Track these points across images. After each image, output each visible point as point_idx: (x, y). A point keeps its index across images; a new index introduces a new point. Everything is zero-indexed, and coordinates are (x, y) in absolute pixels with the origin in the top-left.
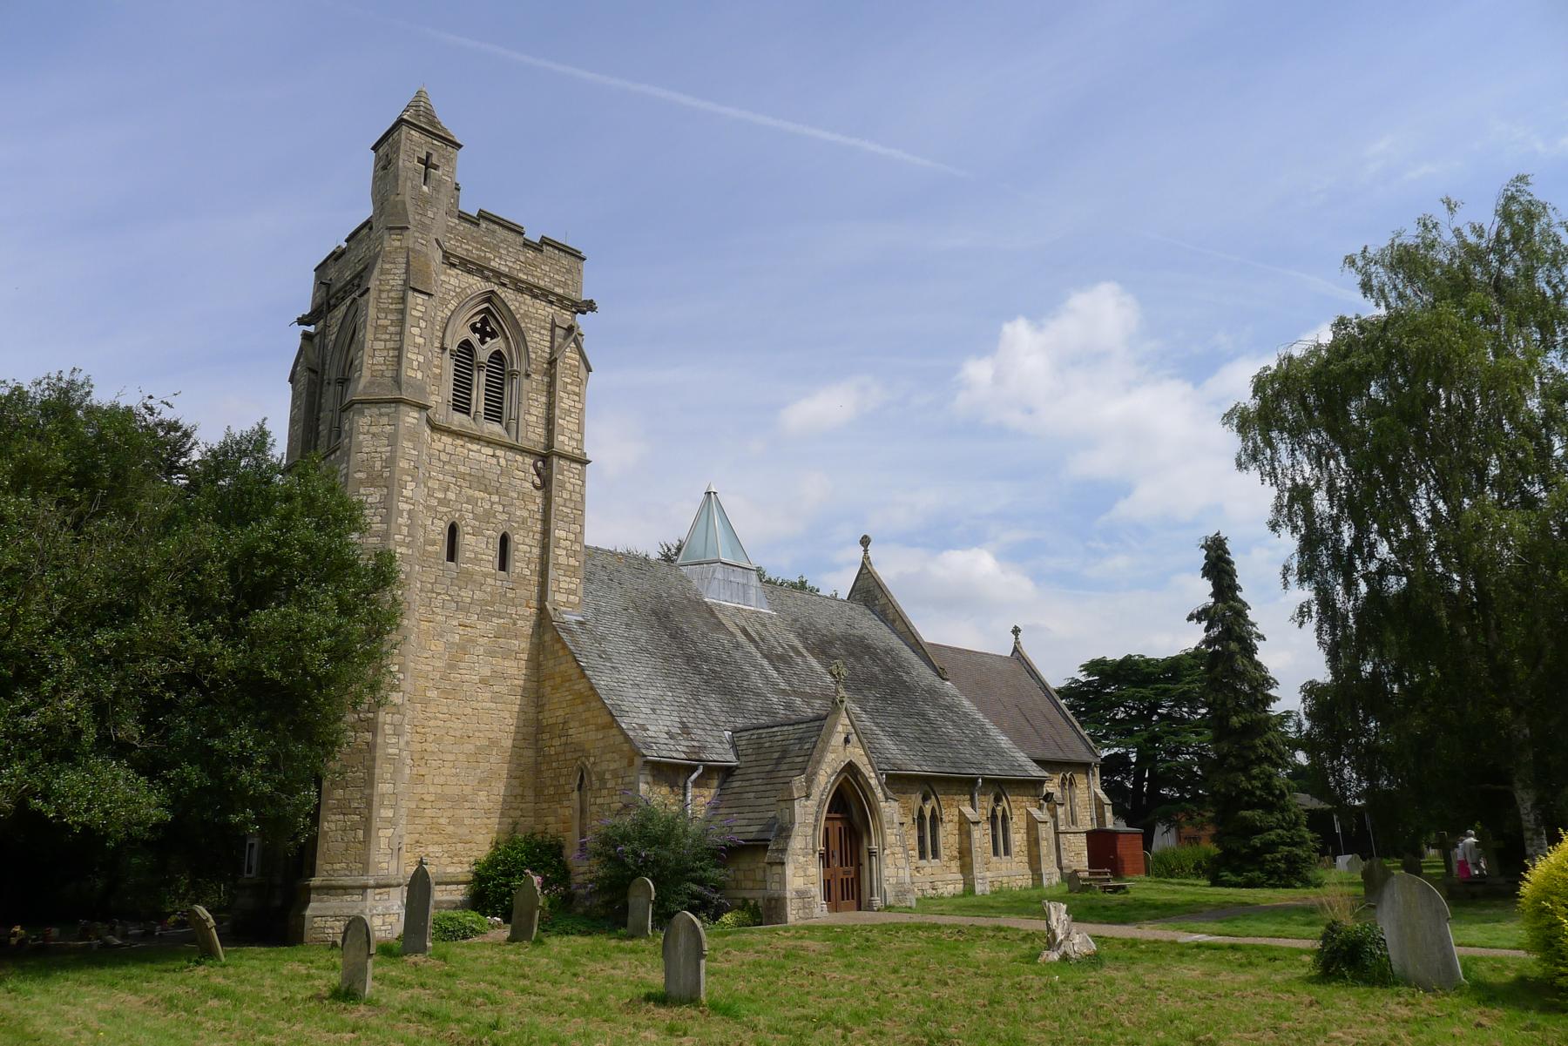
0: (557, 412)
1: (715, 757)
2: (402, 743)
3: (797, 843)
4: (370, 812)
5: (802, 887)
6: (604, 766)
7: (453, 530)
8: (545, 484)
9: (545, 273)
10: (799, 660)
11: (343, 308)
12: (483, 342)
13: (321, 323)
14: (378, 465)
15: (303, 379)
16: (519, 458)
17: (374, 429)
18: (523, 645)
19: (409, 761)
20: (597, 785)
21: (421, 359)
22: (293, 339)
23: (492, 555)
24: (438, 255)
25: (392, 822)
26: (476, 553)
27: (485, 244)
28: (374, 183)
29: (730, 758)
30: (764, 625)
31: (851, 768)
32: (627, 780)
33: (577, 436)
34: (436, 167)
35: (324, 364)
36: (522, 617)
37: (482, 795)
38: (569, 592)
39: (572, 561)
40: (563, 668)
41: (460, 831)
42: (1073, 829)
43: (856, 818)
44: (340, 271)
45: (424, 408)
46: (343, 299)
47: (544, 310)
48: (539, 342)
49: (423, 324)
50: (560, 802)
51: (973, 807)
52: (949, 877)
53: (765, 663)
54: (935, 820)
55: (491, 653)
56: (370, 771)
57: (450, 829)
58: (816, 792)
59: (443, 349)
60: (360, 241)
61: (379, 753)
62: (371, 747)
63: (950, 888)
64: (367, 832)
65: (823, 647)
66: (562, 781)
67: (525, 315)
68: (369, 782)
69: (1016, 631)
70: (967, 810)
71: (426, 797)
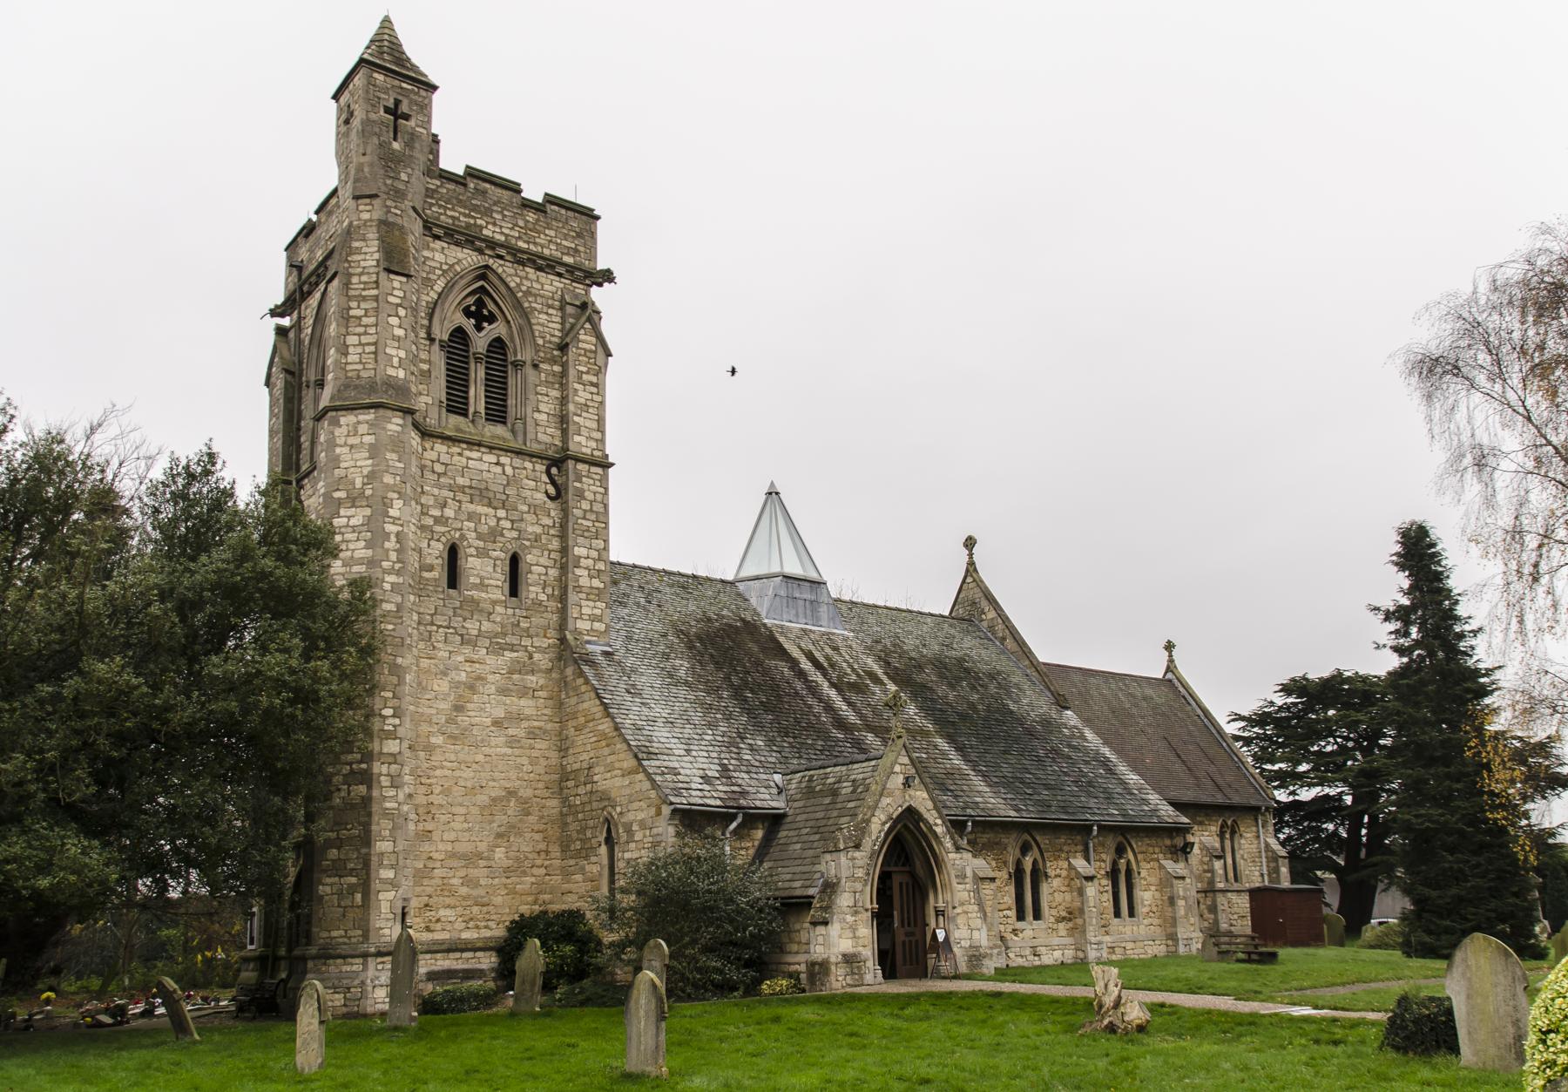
0: (571, 407)
1: (758, 803)
2: (401, 797)
3: (844, 900)
4: (368, 874)
5: (851, 950)
6: (630, 817)
7: (453, 553)
8: (559, 495)
9: (548, 243)
10: (877, 689)
11: (318, 295)
12: (479, 328)
13: (295, 315)
14: (358, 483)
15: (279, 384)
16: (528, 465)
17: (351, 441)
18: (541, 682)
19: (413, 816)
20: (624, 837)
21: (402, 354)
24: (417, 227)
25: (393, 884)
26: (482, 578)
27: (475, 208)
28: (338, 140)
29: (779, 804)
30: (836, 649)
31: (911, 814)
32: (655, 831)
33: (598, 435)
34: (407, 117)
35: (301, 363)
36: (539, 649)
37: (499, 853)
39: (596, 583)
40: (585, 705)
41: (475, 893)
42: (1236, 886)
43: (920, 870)
44: (311, 251)
45: (409, 412)
46: (317, 284)
47: (551, 285)
48: (548, 324)
49: (402, 312)
50: (586, 857)
51: (1088, 860)
52: (1056, 941)
53: (833, 693)
54: (1038, 875)
55: (503, 691)
56: (367, 827)
57: (464, 890)
58: (868, 844)
59: (431, 340)
60: (330, 213)
61: (375, 808)
62: (367, 801)
63: (1057, 954)
65: (906, 674)
66: (589, 834)
67: (528, 293)
68: (366, 840)
70: (1079, 863)
71: (435, 855)
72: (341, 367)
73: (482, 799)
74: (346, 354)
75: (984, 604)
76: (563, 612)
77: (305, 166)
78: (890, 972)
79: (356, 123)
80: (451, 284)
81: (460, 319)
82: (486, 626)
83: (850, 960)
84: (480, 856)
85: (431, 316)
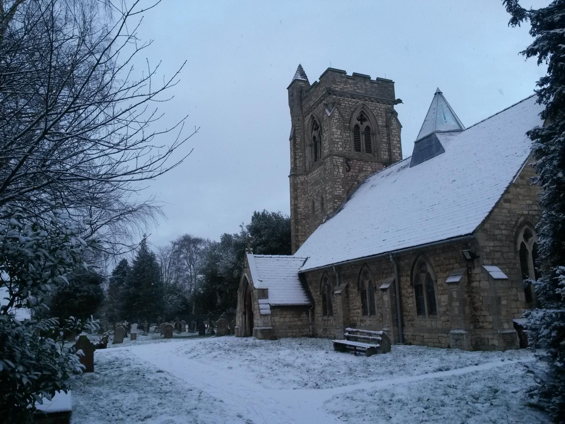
12: (362, 124)
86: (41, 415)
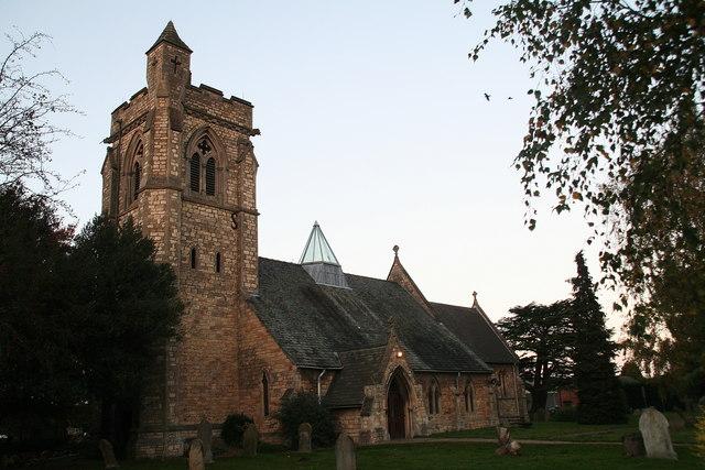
7: (194, 252)
9: (233, 118)
12: (204, 153)
13: (117, 142)
15: (110, 172)
20: (272, 379)
22: (102, 152)
23: (212, 264)
25: (174, 400)
38: (252, 282)
47: (234, 135)
54: (438, 394)
55: (214, 314)
60: (138, 101)
64: (164, 404)
68: (163, 380)
69: (475, 294)
72: (150, 169)
73: (206, 363)
74: (153, 164)
75: (403, 276)
76: (239, 279)
77: (133, 78)
78: (392, 437)
79: (159, 65)
80: (190, 133)
81: (197, 149)
82: (208, 285)
83: (378, 430)
84: (205, 387)
85: (186, 148)
86: (674, 293)
